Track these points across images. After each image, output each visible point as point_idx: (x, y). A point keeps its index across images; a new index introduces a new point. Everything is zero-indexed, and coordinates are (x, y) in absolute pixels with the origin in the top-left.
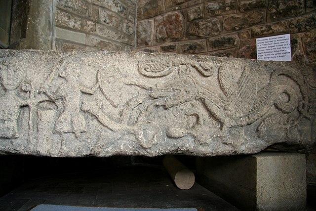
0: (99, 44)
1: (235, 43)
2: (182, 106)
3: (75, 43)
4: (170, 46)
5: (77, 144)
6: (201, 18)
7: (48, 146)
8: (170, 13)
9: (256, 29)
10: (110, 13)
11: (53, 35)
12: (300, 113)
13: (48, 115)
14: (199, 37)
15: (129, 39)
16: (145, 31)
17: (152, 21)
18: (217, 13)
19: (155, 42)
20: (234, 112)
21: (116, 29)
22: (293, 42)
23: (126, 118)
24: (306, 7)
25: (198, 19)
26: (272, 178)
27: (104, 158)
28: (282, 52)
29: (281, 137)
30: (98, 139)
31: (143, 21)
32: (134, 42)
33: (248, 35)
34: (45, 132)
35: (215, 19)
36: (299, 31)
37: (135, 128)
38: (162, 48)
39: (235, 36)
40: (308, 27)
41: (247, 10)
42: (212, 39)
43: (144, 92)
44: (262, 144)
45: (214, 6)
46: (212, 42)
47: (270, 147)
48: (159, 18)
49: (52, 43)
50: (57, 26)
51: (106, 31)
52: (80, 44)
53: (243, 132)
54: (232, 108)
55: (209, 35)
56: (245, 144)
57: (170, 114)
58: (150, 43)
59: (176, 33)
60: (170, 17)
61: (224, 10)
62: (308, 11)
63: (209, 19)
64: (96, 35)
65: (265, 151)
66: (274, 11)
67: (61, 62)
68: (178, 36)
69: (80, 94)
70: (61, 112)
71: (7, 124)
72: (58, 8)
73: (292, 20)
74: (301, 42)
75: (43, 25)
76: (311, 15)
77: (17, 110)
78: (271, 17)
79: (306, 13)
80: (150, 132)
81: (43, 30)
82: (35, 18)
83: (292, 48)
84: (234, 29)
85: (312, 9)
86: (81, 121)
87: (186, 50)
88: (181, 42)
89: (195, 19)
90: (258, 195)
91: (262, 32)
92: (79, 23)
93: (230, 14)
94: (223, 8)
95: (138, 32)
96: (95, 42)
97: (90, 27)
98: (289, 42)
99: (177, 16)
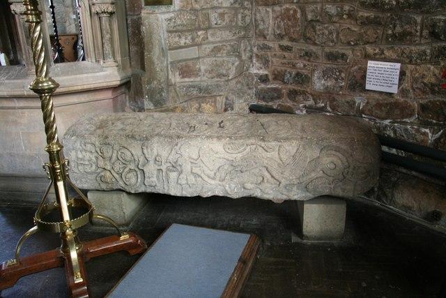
0: (212, 51)
1: (348, 61)
2: (252, 171)
3: (188, 60)
4: (288, 46)
5: (190, 190)
6: (318, 21)
7: (174, 191)
8: (288, 6)
9: (370, 50)
10: (221, 11)
11: (167, 60)
12: (345, 178)
13: (173, 175)
14: (315, 44)
15: (246, 31)
16: (263, 21)
17: (269, 9)
18: (334, 19)
19: (272, 37)
20: (288, 176)
21: (229, 28)
22: (402, 74)
23: (218, 178)
24: (421, 36)
25: (315, 21)
26: (315, 220)
27: (207, 198)
28: (390, 82)
29: (326, 192)
30: (202, 188)
31: (260, 8)
32: (251, 33)
33: (362, 54)
34: (173, 184)
35: (332, 27)
36: (410, 62)
37: (224, 183)
38: (281, 46)
39: (349, 52)
40: (418, 61)
41: (363, 24)
42: (327, 50)
43: (228, 162)
44: (310, 195)
45: (332, 9)
46: (326, 53)
47: (315, 198)
48: (277, 8)
49: (167, 67)
50: (170, 49)
51: (219, 33)
52: (192, 59)
53: (295, 188)
54: (287, 174)
55: (324, 43)
56: (296, 195)
57: (245, 176)
58: (268, 37)
59: (293, 33)
60: (288, 10)
61: (341, 18)
62: (422, 42)
63: (326, 25)
64: (209, 43)
65: (313, 201)
66: (390, 32)
67: (177, 145)
68: (295, 36)
69: (190, 164)
70: (181, 173)
71: (151, 179)
72: (169, 32)
73: (405, 48)
74: (409, 75)
75: (157, 55)
76: (423, 48)
77: (155, 172)
78: (387, 39)
79: (420, 44)
80: (233, 186)
81: (158, 58)
82: (150, 52)
83: (400, 80)
84: (349, 43)
85: (427, 41)
86: (192, 179)
87: (302, 55)
88: (298, 44)
89: (312, 20)
90: (304, 227)
91: (375, 54)
92: (189, 38)
93: (347, 24)
94: (340, 15)
95: (256, 20)
96: (208, 50)
97: (201, 37)
98: (398, 73)
99: (295, 11)
